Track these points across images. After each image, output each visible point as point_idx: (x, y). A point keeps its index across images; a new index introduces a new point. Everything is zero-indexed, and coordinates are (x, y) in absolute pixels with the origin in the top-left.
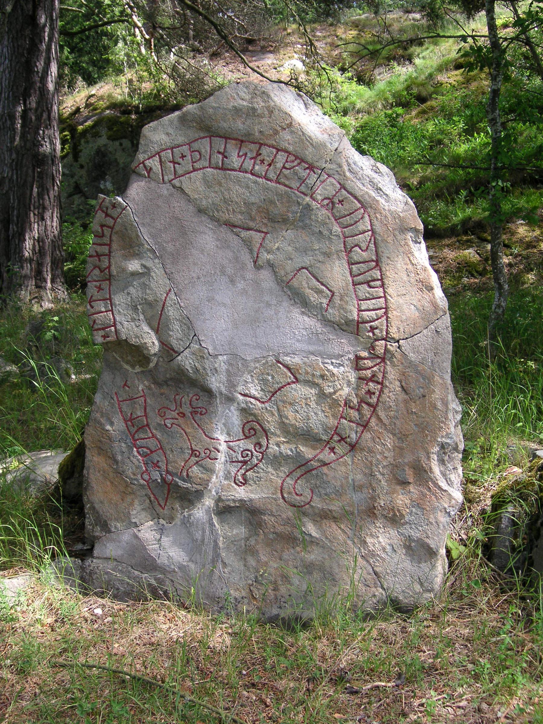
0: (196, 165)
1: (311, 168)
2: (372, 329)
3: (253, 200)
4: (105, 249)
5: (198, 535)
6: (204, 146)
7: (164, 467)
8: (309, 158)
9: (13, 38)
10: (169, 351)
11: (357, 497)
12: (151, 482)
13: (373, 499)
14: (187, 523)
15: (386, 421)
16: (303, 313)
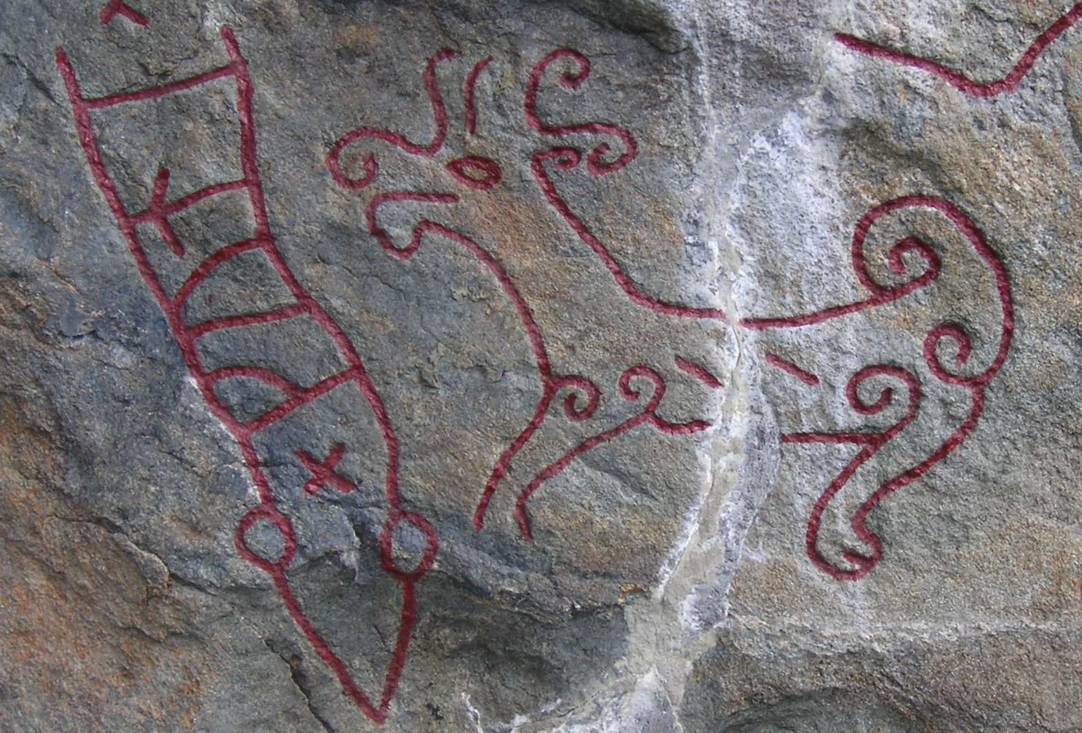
7: (365, 465)
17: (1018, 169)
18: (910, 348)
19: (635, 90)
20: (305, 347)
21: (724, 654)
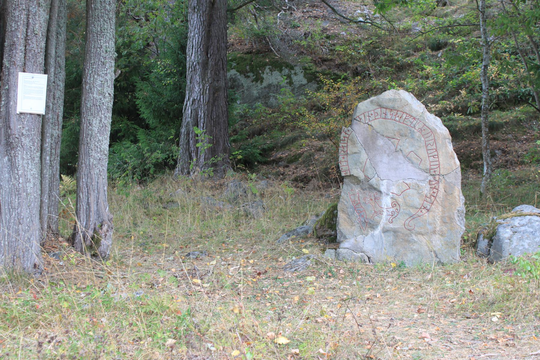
0: (376, 117)
1: (414, 118)
2: (435, 171)
3: (395, 129)
4: (346, 145)
5: (377, 240)
6: (379, 110)
7: (365, 216)
8: (414, 116)
9: (200, 16)
10: (367, 179)
11: (429, 227)
12: (361, 221)
13: (435, 228)
14: (373, 236)
15: (440, 202)
16: (328, 211)
17: (400, 200)
18: (394, 210)
19: (73, 228)
20: (362, 209)
21: (384, 227)
